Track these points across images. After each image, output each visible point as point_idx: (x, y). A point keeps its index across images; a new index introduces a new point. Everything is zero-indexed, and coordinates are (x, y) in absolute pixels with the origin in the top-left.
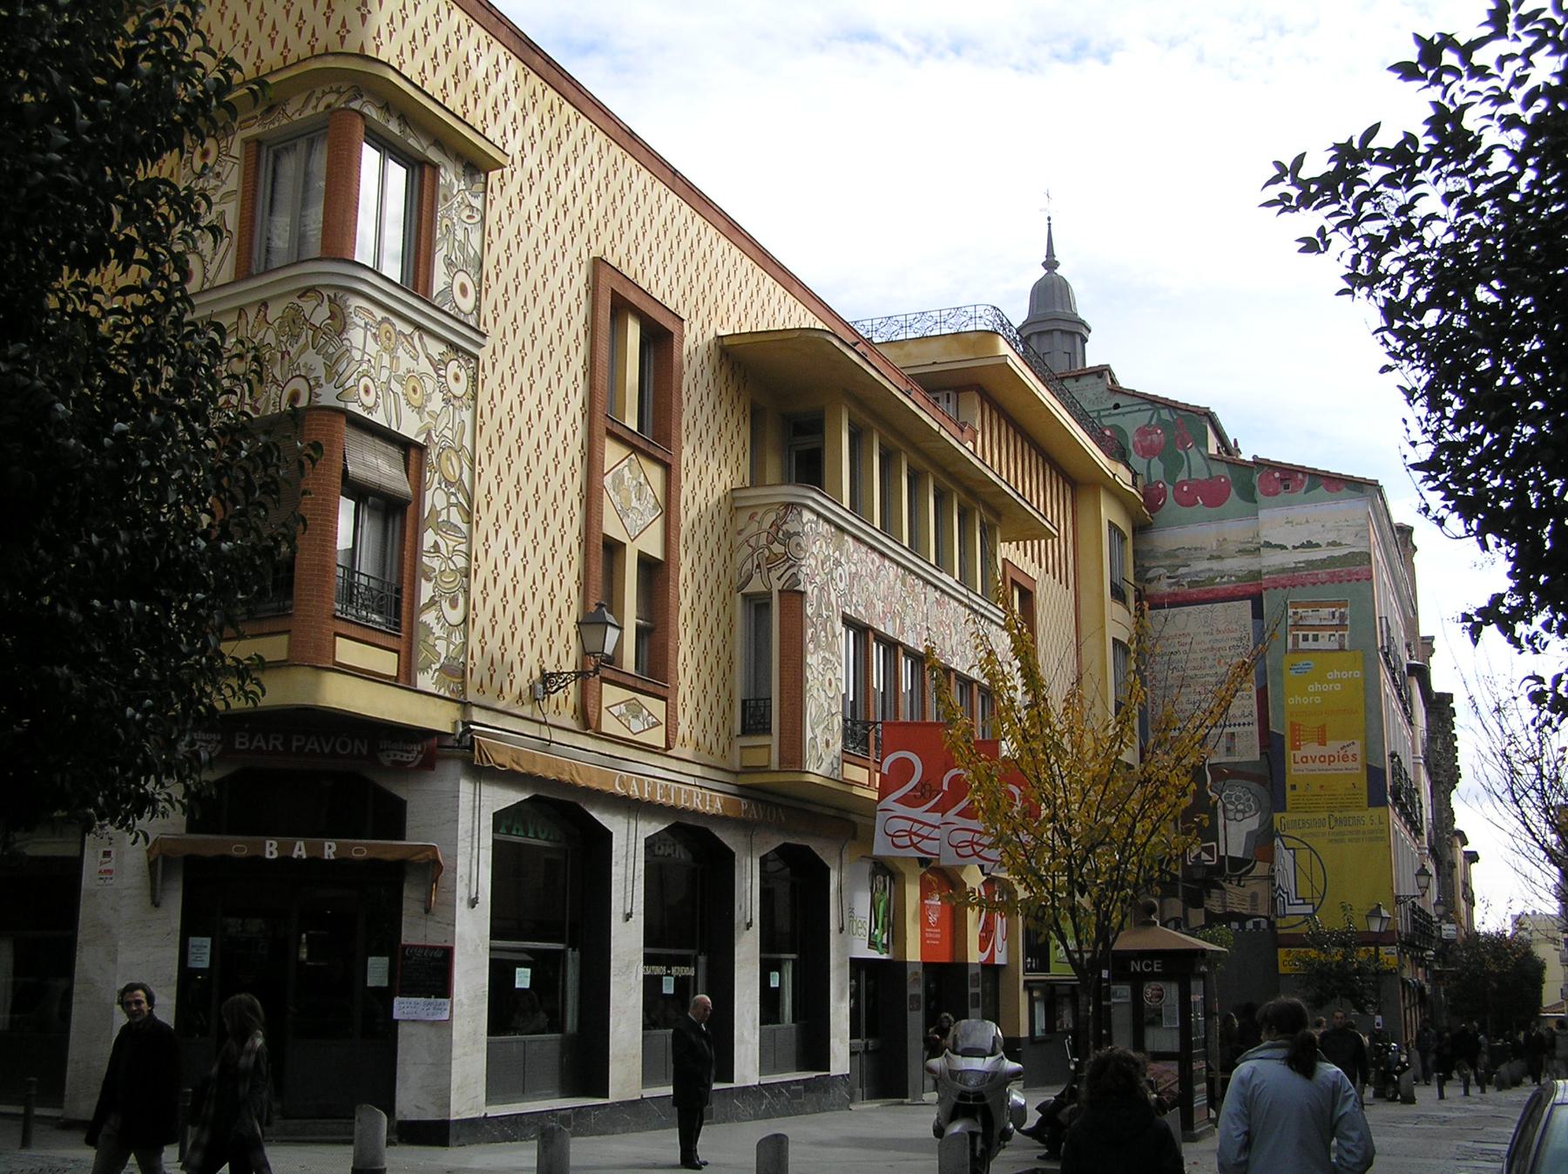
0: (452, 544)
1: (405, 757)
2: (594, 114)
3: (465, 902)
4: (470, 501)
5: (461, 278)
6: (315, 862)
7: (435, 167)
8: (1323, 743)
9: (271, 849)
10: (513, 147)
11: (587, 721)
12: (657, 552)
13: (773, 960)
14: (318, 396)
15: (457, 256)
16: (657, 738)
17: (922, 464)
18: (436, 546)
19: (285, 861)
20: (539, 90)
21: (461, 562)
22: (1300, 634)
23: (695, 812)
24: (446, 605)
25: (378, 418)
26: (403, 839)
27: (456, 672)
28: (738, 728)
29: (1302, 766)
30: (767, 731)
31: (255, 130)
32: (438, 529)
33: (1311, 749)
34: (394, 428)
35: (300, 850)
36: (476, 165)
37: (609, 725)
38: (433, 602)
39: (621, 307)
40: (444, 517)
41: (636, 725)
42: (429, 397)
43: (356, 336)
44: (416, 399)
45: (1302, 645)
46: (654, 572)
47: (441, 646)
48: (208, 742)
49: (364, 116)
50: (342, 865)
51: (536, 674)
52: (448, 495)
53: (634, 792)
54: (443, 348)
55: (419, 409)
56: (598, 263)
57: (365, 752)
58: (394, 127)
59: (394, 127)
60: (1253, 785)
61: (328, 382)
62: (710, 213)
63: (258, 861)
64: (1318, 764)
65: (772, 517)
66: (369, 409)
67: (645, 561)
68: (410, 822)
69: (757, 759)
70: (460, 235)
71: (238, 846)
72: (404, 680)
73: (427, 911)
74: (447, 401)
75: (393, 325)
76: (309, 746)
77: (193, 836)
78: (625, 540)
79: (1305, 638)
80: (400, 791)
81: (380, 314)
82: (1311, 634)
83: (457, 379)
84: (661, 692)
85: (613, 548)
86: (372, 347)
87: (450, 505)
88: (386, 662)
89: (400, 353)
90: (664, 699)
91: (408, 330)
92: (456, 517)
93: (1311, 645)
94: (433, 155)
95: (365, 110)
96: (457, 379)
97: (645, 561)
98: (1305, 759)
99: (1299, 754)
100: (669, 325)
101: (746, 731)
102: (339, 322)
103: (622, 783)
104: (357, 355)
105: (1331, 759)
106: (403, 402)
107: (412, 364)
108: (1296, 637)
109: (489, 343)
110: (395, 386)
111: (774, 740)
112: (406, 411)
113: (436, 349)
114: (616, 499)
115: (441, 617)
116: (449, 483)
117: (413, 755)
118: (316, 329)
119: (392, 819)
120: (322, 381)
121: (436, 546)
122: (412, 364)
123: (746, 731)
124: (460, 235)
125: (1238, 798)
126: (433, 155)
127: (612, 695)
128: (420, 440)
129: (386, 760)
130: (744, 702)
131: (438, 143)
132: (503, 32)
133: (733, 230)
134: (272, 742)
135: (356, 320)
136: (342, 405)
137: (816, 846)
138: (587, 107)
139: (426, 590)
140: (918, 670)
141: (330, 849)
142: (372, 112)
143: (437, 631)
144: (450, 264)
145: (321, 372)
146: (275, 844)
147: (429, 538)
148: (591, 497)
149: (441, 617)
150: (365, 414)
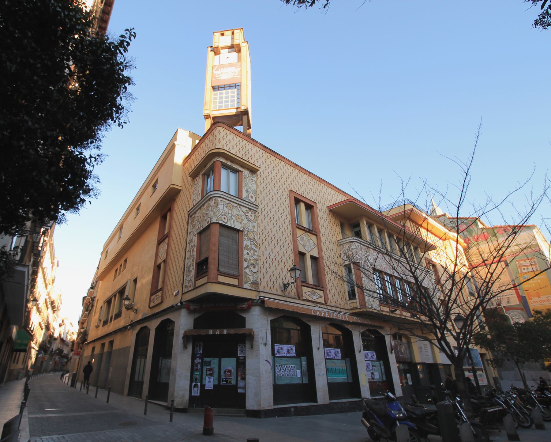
2: (285, 160)
5: (251, 194)
6: (222, 335)
8: (539, 297)
9: (211, 332)
11: (299, 296)
12: (316, 255)
13: (236, 335)
15: (249, 190)
16: (322, 300)
17: (382, 227)
18: (248, 254)
19: (214, 335)
20: (247, 144)
22: (522, 268)
23: (339, 320)
24: (252, 268)
25: (228, 224)
27: (255, 283)
28: (348, 298)
29: (533, 304)
30: (355, 298)
31: (203, 172)
32: (248, 249)
33: (536, 299)
35: (218, 332)
36: (253, 171)
38: (247, 267)
39: (297, 201)
40: (250, 247)
41: (314, 297)
42: (243, 220)
43: (220, 207)
44: (240, 220)
45: (524, 271)
47: (251, 278)
50: (228, 335)
51: (282, 284)
52: (251, 242)
54: (247, 209)
55: (241, 223)
56: (291, 191)
58: (229, 163)
59: (229, 163)
60: (520, 311)
63: (208, 335)
64: (539, 303)
65: (348, 246)
66: (226, 222)
67: (313, 258)
69: (354, 305)
70: (250, 185)
71: (203, 332)
73: (252, 347)
74: (249, 221)
78: (306, 252)
79: (524, 269)
80: (244, 315)
81: (227, 202)
82: (525, 268)
83: (251, 216)
84: (322, 289)
85: (302, 255)
86: (225, 209)
87: (251, 244)
88: (235, 282)
89: (234, 210)
90: (323, 291)
91: (236, 205)
92: (253, 247)
93: (526, 271)
96: (251, 216)
97: (313, 258)
98: (534, 302)
99: (532, 301)
101: (350, 299)
102: (217, 204)
105: (544, 301)
107: (238, 213)
108: (521, 269)
109: (260, 208)
110: (233, 217)
111: (357, 301)
112: (236, 223)
113: (245, 210)
114: (302, 243)
115: (251, 271)
116: (250, 239)
117: (245, 306)
118: (211, 206)
119: (242, 322)
121: (248, 254)
122: (238, 213)
123: (350, 299)
124: (250, 185)
125: (516, 315)
127: (305, 289)
128: (241, 229)
129: (239, 307)
130: (349, 292)
131: (242, 166)
132: (268, 150)
133: (302, 169)
137: (378, 330)
138: (283, 159)
139: (245, 264)
140: (401, 282)
143: (249, 274)
144: (247, 192)
145: (213, 215)
147: (245, 252)
148: (295, 242)
149: (251, 271)
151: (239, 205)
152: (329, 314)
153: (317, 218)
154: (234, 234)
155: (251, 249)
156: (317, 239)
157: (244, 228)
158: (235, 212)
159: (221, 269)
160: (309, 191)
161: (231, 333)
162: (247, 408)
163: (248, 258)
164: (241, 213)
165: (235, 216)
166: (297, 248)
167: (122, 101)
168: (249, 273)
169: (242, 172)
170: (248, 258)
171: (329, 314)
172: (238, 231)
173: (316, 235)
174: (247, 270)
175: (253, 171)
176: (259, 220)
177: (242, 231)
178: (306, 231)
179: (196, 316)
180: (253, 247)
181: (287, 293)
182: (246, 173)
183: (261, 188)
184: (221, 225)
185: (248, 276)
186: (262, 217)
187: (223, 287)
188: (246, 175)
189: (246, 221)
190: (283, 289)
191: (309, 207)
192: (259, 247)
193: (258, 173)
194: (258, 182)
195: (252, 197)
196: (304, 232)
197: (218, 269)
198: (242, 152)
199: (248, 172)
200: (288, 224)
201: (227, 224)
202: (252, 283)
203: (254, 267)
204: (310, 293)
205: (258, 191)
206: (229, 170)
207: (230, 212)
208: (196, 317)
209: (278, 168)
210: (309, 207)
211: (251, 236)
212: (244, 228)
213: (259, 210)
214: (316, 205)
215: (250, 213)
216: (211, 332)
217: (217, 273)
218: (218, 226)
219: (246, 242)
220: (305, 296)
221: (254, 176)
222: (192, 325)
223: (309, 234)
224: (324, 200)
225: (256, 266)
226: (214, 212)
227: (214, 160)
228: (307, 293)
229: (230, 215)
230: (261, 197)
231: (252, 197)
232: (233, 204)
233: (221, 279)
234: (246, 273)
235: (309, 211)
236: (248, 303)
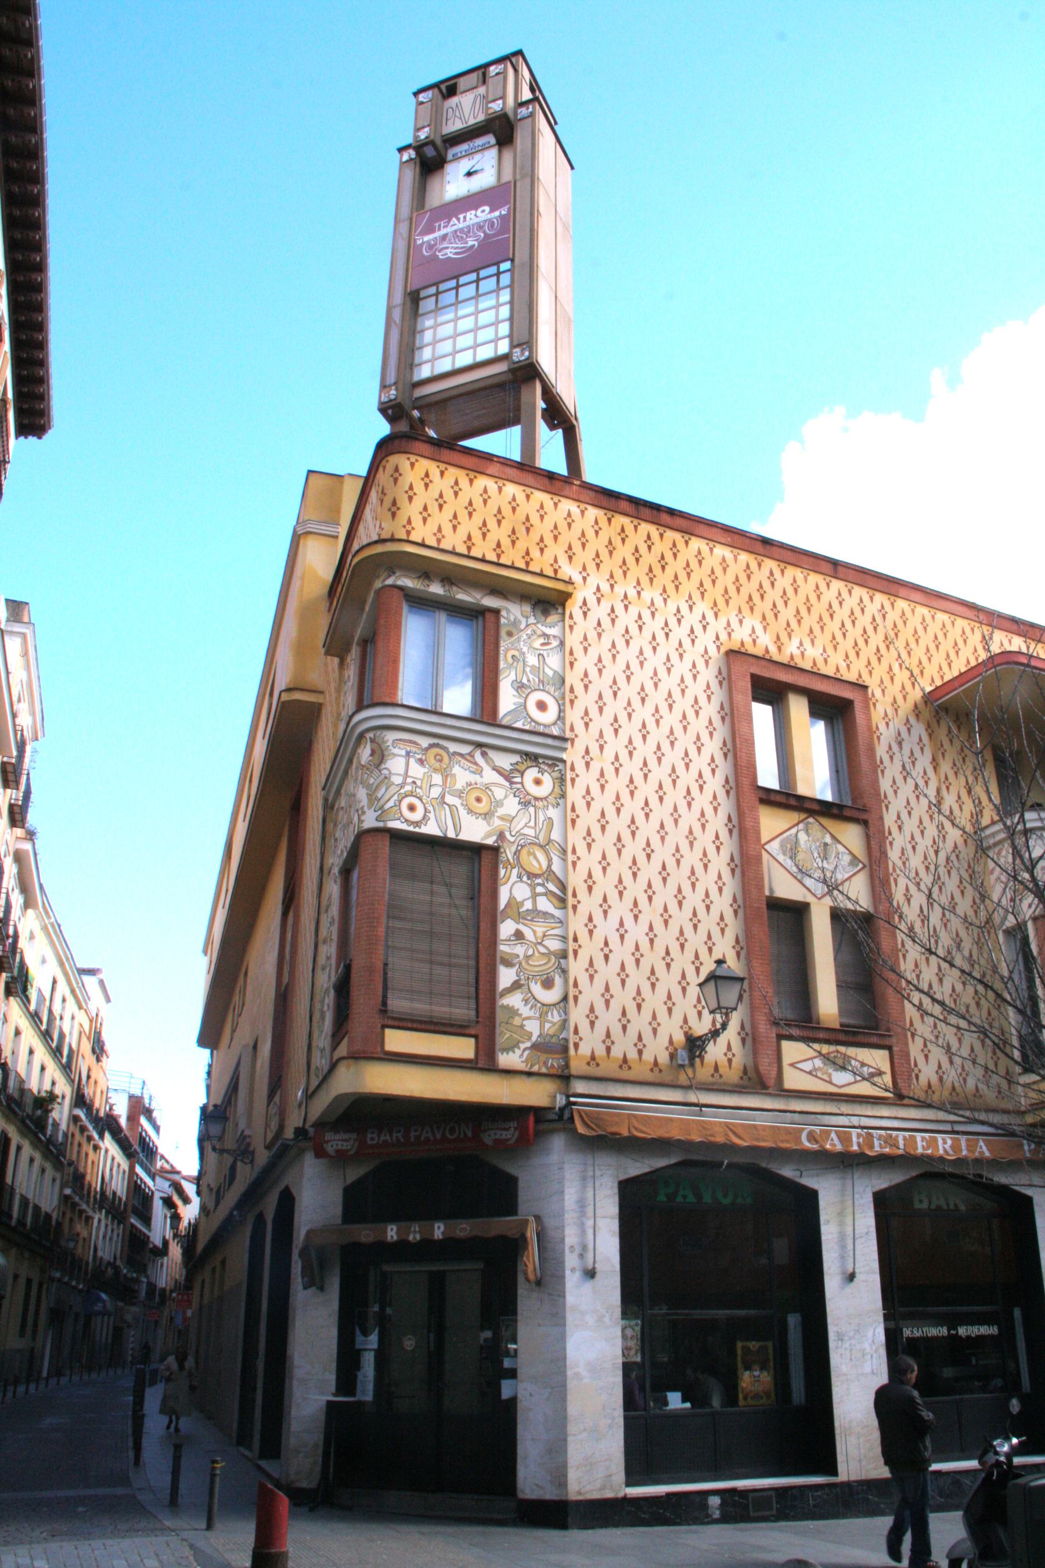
0: (540, 931)
1: (504, 1135)
3: (578, 1274)
4: (563, 887)
7: (497, 612)
10: (568, 571)
11: (758, 1080)
14: (363, 821)
18: (519, 935)
21: (554, 945)
24: (537, 989)
25: (431, 829)
26: (516, 1214)
27: (556, 1047)
32: (519, 917)
34: (451, 834)
36: (549, 601)
37: (793, 1080)
38: (516, 986)
40: (528, 905)
42: (499, 804)
43: (396, 765)
44: (483, 807)
46: (857, 930)
47: (533, 1027)
48: (346, 1141)
49: (401, 588)
52: (533, 887)
53: (833, 1144)
54: (516, 758)
55: (487, 816)
57: (469, 1134)
58: (436, 589)
59: (436, 589)
61: (369, 808)
62: (679, 522)
66: (417, 824)
68: (522, 1196)
70: (532, 660)
71: (365, 1234)
72: (485, 1063)
74: (525, 804)
75: (445, 749)
76: (424, 1135)
77: (346, 1226)
78: (810, 899)
80: (511, 1169)
81: (424, 742)
85: (791, 916)
86: (417, 771)
87: (534, 896)
88: (463, 1048)
91: (465, 749)
92: (544, 904)
94: (490, 602)
95: (399, 583)
96: (538, 782)
100: (846, 694)
102: (380, 756)
103: (811, 1137)
104: (397, 780)
106: (463, 812)
110: (449, 799)
113: (505, 761)
115: (530, 999)
116: (531, 876)
117: (509, 1134)
119: (504, 1195)
120: (366, 809)
121: (519, 935)
124: (532, 660)
126: (490, 602)
128: (490, 841)
129: (488, 1139)
134: (394, 1135)
135: (396, 751)
136: (381, 825)
139: (506, 977)
141: (439, 1230)
142: (408, 582)
143: (525, 1011)
144: (519, 686)
145: (365, 801)
146: (395, 1228)
147: (506, 928)
148: (747, 863)
150: (411, 829)
151: (480, 745)
152: (956, 1147)
153: (871, 750)
154: (459, 870)
155: (536, 914)
156: (868, 838)
157: (501, 836)
158: (462, 775)
159: (397, 1004)
160: (818, 639)
161: (363, 1240)
162: (521, 1496)
163: (520, 950)
164: (490, 776)
165: (459, 794)
166: (760, 887)
167: (30, 438)
168: (525, 1011)
169: (497, 612)
170: (520, 950)
171: (892, 1142)
172: (475, 851)
173: (865, 823)
174: (514, 1001)
175: (549, 601)
176: (575, 794)
177: (495, 851)
178: (811, 813)
179: (354, 1174)
180: (544, 904)
181: (703, 1073)
182: (513, 612)
183: (585, 662)
184: (398, 837)
185: (517, 1021)
186: (586, 779)
187: (416, 1070)
188: (516, 623)
189: (511, 805)
190: (683, 1056)
191: (835, 708)
192: (571, 901)
193: (574, 607)
194: (573, 640)
195: (542, 706)
196: (803, 816)
197: (384, 1003)
198: (499, 533)
199: (527, 608)
200: (895, 830)
201: (425, 830)
202: (535, 1047)
203: (548, 984)
204: (818, 1063)
205: (573, 678)
206: (442, 616)
207: (437, 779)
208: (349, 1181)
209: (773, 595)
210: (835, 708)
211: (538, 861)
212: (501, 836)
213: (572, 755)
214: (866, 700)
215: (532, 773)
216: (392, 1233)
217: (378, 1021)
218: (384, 846)
219: (512, 889)
220: (793, 1080)
221: (553, 618)
222: (338, 1211)
223: (825, 821)
224: (901, 667)
225: (558, 980)
226: (368, 787)
227: (378, 584)
228: (807, 1066)
229: (435, 792)
230: (586, 700)
231: (542, 706)
232: (453, 747)
233: (397, 1040)
234: (513, 1012)
235: (840, 726)
236: (528, 1125)
